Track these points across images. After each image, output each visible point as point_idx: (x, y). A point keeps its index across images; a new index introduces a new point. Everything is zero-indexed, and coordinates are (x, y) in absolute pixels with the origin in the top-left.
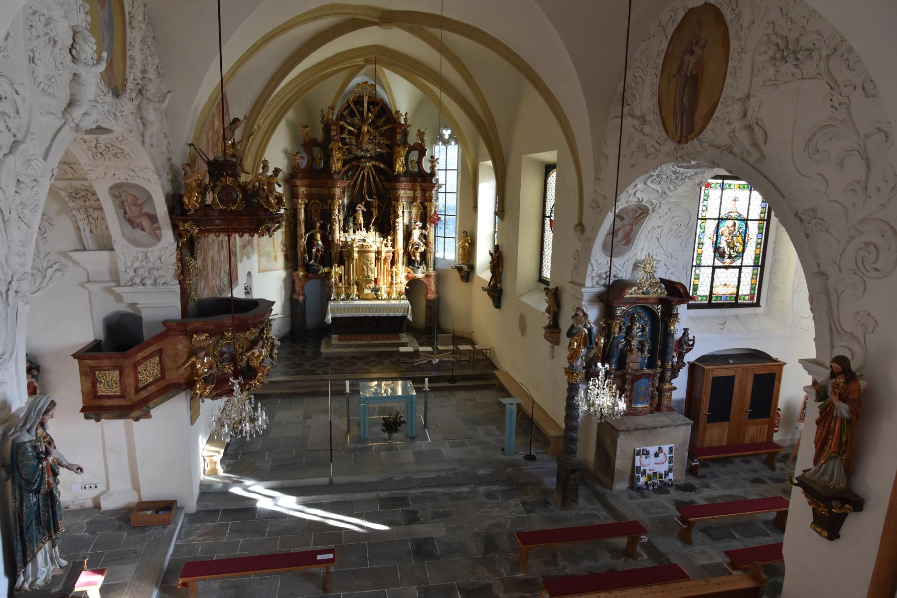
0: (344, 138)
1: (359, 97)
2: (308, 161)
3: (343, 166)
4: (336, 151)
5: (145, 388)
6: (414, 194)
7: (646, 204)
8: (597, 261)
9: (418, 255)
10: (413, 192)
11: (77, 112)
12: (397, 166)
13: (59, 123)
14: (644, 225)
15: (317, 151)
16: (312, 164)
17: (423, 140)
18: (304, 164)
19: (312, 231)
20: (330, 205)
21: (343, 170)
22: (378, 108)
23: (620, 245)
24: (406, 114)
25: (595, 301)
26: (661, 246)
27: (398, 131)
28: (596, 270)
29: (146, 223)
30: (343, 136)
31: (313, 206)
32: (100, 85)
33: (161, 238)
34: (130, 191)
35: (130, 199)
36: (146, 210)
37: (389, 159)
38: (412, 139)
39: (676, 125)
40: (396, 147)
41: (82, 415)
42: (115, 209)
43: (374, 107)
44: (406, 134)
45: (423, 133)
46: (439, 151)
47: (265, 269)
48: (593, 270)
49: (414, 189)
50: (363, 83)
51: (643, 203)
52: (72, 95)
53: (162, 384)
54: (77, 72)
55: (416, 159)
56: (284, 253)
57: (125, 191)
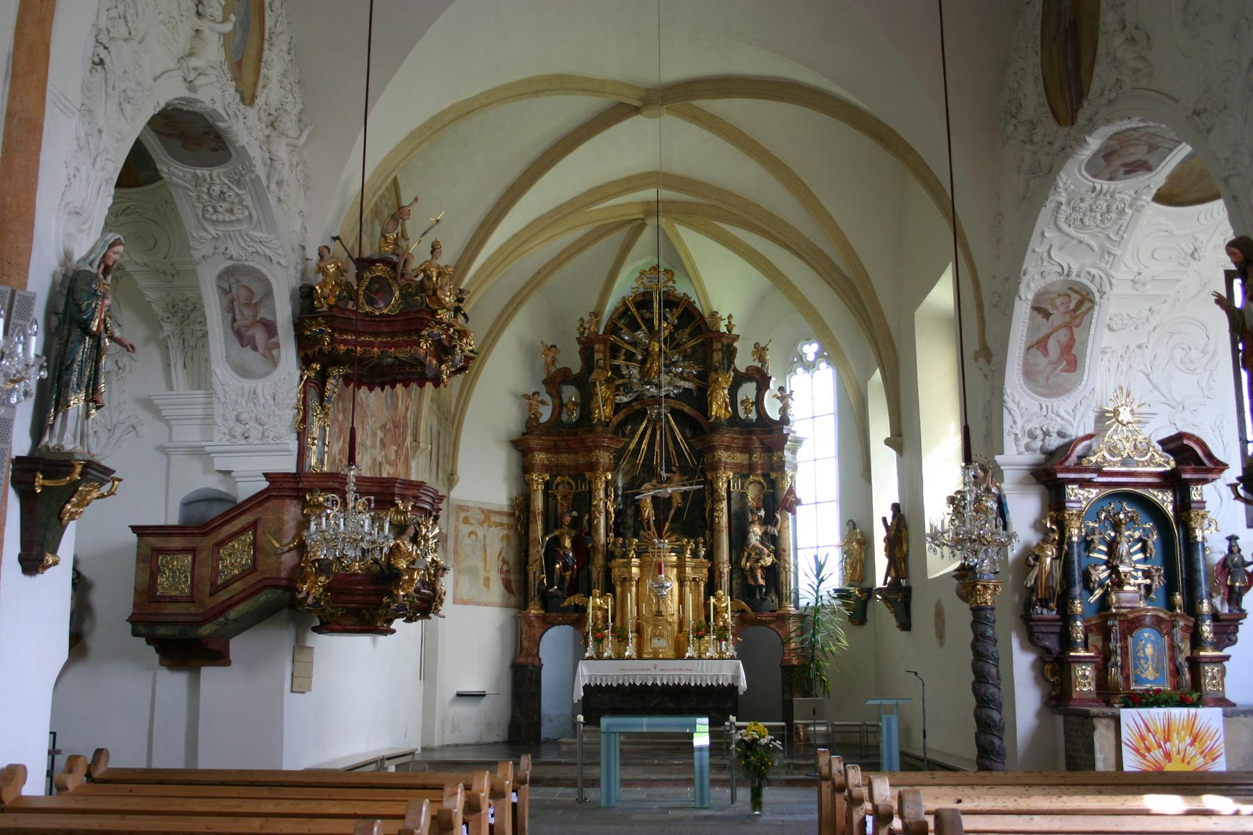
0: (618, 367)
1: (644, 294)
2: (553, 409)
3: (616, 412)
4: (601, 385)
5: (226, 585)
6: (750, 458)
7: (1078, 280)
8: (1018, 404)
9: (759, 573)
10: (747, 456)
11: (194, 62)
12: (714, 407)
13: (172, 65)
14: (1093, 326)
15: (570, 393)
16: (560, 414)
17: (762, 359)
18: (546, 414)
19: (557, 533)
20: (590, 483)
21: (615, 420)
22: (677, 312)
23: (1058, 371)
24: (730, 317)
25: (1028, 484)
26: (1156, 388)
27: (715, 347)
28: (1018, 420)
29: (259, 335)
30: (617, 362)
31: (560, 487)
32: (223, 66)
33: (279, 362)
34: (245, 281)
35: (243, 294)
36: (263, 314)
37: (701, 398)
38: (743, 361)
39: (1066, 105)
40: (713, 373)
41: (129, 626)
42: (222, 314)
43: (671, 311)
44: (730, 353)
45: (764, 349)
46: (799, 382)
47: (465, 598)
48: (1015, 422)
49: (747, 449)
50: (651, 269)
51: (1073, 277)
52: (191, 48)
53: (252, 579)
54: (200, 28)
55: (752, 398)
56: (503, 576)
57: (238, 281)
